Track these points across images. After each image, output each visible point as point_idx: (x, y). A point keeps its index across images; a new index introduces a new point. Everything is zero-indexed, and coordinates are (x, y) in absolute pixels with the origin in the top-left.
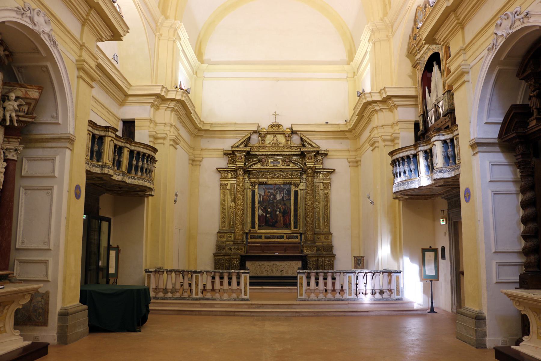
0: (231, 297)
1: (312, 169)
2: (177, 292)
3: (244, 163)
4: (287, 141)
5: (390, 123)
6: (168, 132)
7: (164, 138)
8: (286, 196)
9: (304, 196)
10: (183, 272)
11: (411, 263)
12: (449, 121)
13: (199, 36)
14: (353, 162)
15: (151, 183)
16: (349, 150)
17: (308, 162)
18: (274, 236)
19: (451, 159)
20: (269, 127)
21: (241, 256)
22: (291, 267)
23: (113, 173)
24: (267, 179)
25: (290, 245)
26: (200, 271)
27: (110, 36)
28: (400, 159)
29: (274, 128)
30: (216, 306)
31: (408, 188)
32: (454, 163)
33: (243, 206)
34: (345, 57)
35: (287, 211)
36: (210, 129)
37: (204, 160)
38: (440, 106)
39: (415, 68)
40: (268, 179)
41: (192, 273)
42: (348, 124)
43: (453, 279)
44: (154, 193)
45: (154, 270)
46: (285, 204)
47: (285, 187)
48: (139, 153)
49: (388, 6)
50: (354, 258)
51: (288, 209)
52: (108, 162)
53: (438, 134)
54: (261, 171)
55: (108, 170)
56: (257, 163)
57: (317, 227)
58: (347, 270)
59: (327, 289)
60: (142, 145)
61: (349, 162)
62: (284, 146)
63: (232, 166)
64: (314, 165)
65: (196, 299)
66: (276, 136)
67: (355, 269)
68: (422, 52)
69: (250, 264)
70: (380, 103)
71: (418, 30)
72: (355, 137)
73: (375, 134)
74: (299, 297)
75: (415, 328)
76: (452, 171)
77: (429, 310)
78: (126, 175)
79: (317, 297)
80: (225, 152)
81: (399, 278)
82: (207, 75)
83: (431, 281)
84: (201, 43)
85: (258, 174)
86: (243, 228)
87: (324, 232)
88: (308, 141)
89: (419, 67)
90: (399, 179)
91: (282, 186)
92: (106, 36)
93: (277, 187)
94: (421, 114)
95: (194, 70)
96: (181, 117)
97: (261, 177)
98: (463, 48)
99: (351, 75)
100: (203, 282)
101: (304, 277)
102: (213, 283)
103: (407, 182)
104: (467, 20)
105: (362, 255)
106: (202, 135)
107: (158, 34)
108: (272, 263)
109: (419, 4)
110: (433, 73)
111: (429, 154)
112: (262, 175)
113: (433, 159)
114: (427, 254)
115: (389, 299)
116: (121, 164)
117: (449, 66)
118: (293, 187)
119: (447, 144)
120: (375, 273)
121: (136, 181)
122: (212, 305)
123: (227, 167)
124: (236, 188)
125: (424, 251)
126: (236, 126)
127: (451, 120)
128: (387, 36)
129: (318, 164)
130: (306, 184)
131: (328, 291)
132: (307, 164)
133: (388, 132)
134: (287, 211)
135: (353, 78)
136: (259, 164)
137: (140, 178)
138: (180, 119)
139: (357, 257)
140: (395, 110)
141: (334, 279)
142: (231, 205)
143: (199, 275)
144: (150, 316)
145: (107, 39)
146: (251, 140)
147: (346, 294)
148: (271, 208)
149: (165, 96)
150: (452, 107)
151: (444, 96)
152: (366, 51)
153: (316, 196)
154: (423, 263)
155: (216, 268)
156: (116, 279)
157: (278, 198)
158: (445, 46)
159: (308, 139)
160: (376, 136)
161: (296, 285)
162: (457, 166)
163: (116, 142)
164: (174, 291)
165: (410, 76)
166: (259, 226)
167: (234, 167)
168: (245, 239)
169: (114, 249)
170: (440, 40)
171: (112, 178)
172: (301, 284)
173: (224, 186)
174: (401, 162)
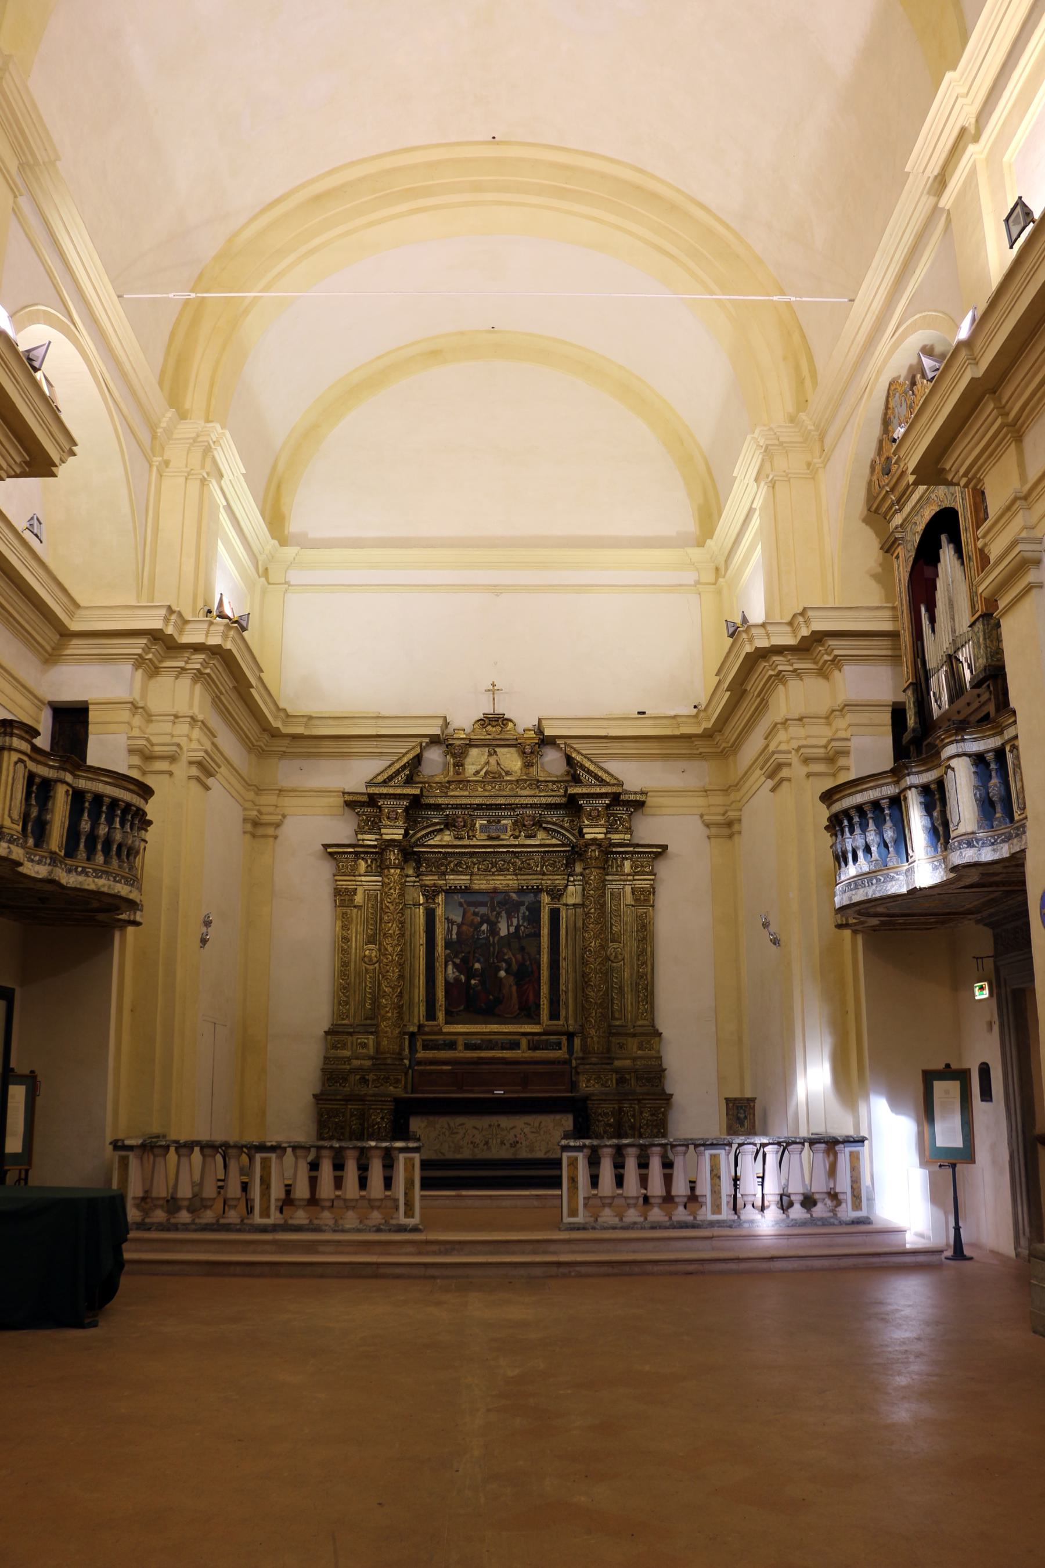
0: (367, 1222)
1: (600, 846)
2: (206, 1207)
3: (402, 831)
4: (528, 765)
5: (823, 709)
6: (185, 739)
7: (173, 758)
8: (525, 924)
9: (577, 925)
10: (223, 1149)
11: (893, 1115)
12: (990, 699)
13: (274, 468)
14: (718, 825)
15: (132, 885)
16: (706, 791)
17: (587, 826)
18: (490, 1041)
19: (999, 808)
20: (476, 726)
21: (397, 1101)
22: (542, 1132)
23: (21, 856)
24: (471, 875)
25: (540, 1068)
26: (274, 1144)
27: (20, 465)
28: (853, 813)
29: (489, 728)
30: (321, 1248)
31: (878, 895)
32: (1008, 820)
33: (401, 954)
34: (690, 525)
35: (530, 969)
36: (306, 733)
37: (287, 821)
38: (962, 659)
39: (889, 554)
40: (474, 878)
41: (253, 1152)
42: (702, 715)
43: (1016, 1161)
44: (141, 916)
45: (140, 1141)
46: (522, 949)
47: (522, 899)
48: (98, 798)
49: (808, 382)
50: (727, 1104)
51: (531, 964)
52: (7, 822)
53: (959, 738)
54: (454, 853)
55: (9, 848)
56: (441, 830)
57: (617, 1015)
58: (706, 1136)
59: (648, 1194)
60: (108, 776)
61: (708, 826)
62: (517, 781)
63: (370, 839)
64: (605, 834)
65: (264, 1229)
66: (495, 752)
67: (729, 1134)
68: (907, 509)
69: (423, 1125)
70: (792, 655)
71: (895, 446)
72: (722, 752)
73: (780, 743)
74: (567, 1220)
75: (909, 1306)
76: (1003, 841)
77: (950, 1253)
78: (61, 862)
79: (621, 1220)
80: (347, 798)
81: (858, 1159)
82: (296, 577)
83: (953, 1166)
84: (279, 486)
85: (443, 861)
86: (402, 1019)
87: (639, 1030)
88: (587, 764)
89: (900, 550)
90: (851, 870)
91: (514, 896)
92: (9, 465)
93: (500, 898)
94: (911, 684)
95: (260, 563)
96: (222, 697)
97: (452, 870)
98: (1022, 495)
99: (708, 576)
100: (284, 1179)
101: (581, 1158)
102: (313, 1182)
103: (876, 877)
104: (1028, 417)
105: (748, 1094)
106: (284, 749)
107: (157, 460)
108: (485, 1122)
109: (895, 375)
110: (941, 567)
111: (937, 796)
112: (456, 865)
113: (948, 808)
114: (939, 1086)
115: (832, 1220)
116: (47, 832)
117: (985, 545)
118: (546, 899)
119: (987, 765)
120: (788, 1144)
121: (90, 879)
122: (311, 1247)
123: (354, 842)
124: (382, 904)
125: (929, 1077)
126: (381, 722)
127: (997, 698)
128: (809, 465)
129: (617, 831)
130: (584, 890)
131: (652, 1200)
132: (585, 831)
133: (818, 735)
134: (530, 969)
135: (715, 584)
136: (448, 832)
137: (103, 872)
138: (217, 702)
139: (735, 1099)
140: (836, 673)
141: (668, 1165)
142: (367, 953)
143: (273, 1156)
144: (124, 1281)
145: (13, 473)
146: (423, 763)
147: (704, 1208)
148: (482, 959)
149: (176, 636)
150: (998, 660)
151: (973, 630)
152: (751, 507)
153: (611, 924)
154: (927, 1113)
155: (320, 1137)
156: (27, 1171)
157: (503, 932)
158: (972, 490)
159: (589, 760)
160: (783, 747)
161: (558, 1185)
162: (1018, 828)
163: (32, 766)
164: (197, 1204)
165: (876, 577)
166: (448, 1013)
167: (376, 843)
168: (407, 1050)
169: (20, 1079)
170: (957, 472)
171: (20, 869)
172: (573, 1180)
173: (347, 898)
174: (856, 819)
